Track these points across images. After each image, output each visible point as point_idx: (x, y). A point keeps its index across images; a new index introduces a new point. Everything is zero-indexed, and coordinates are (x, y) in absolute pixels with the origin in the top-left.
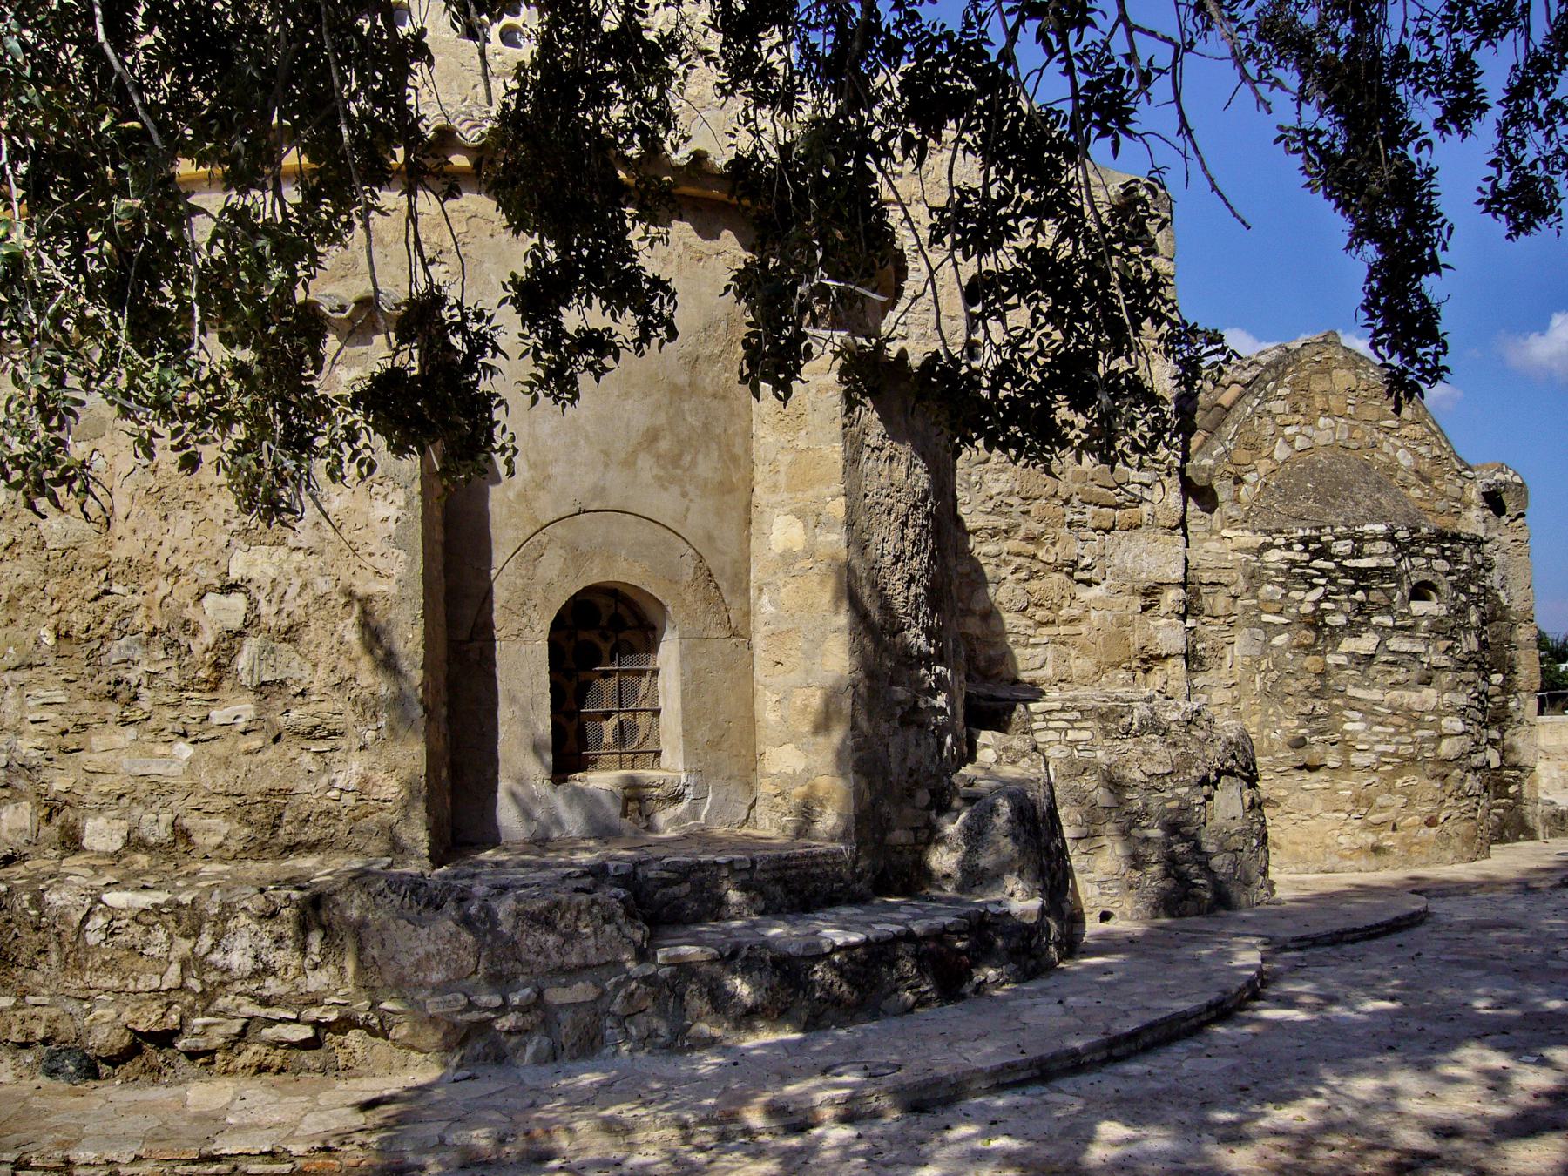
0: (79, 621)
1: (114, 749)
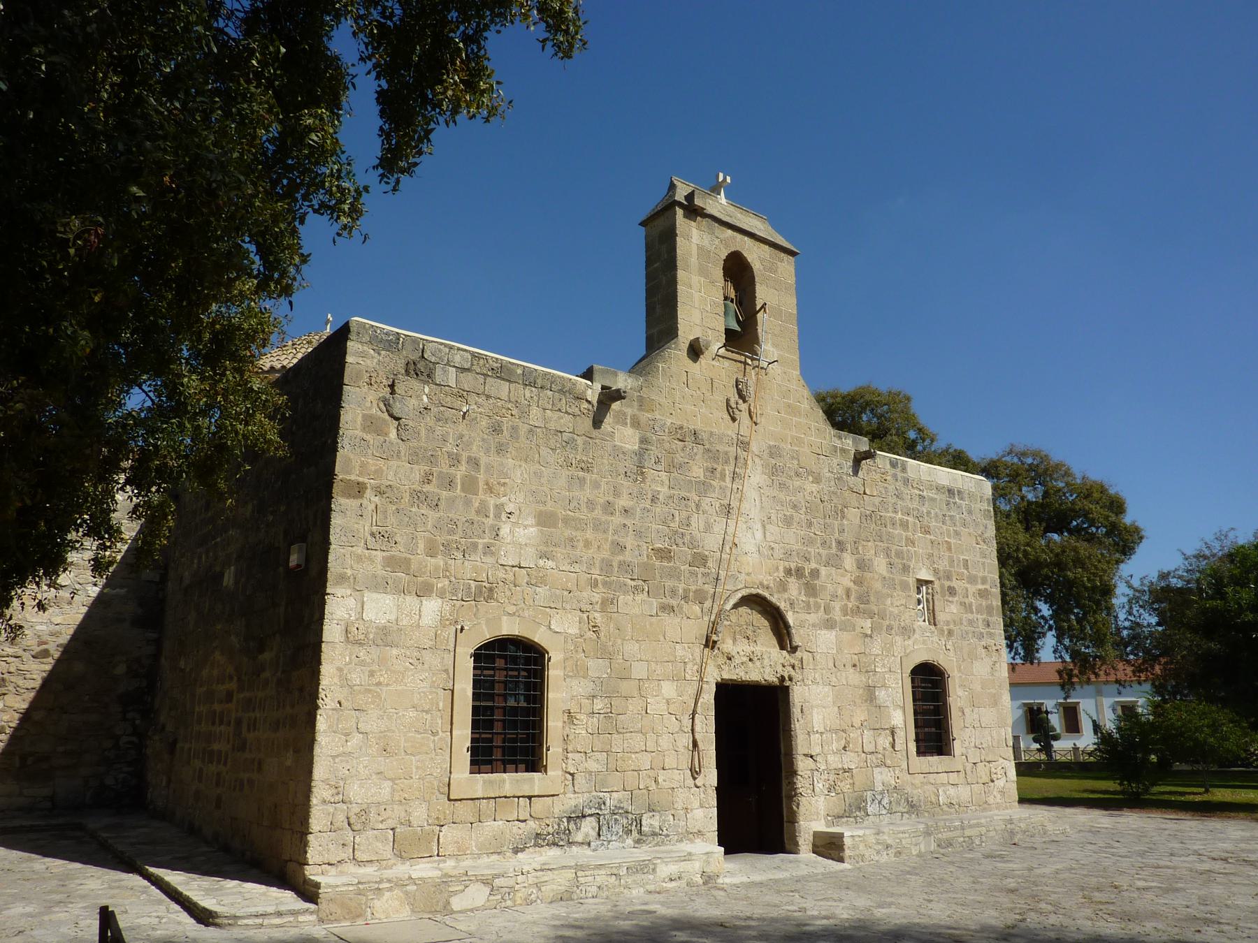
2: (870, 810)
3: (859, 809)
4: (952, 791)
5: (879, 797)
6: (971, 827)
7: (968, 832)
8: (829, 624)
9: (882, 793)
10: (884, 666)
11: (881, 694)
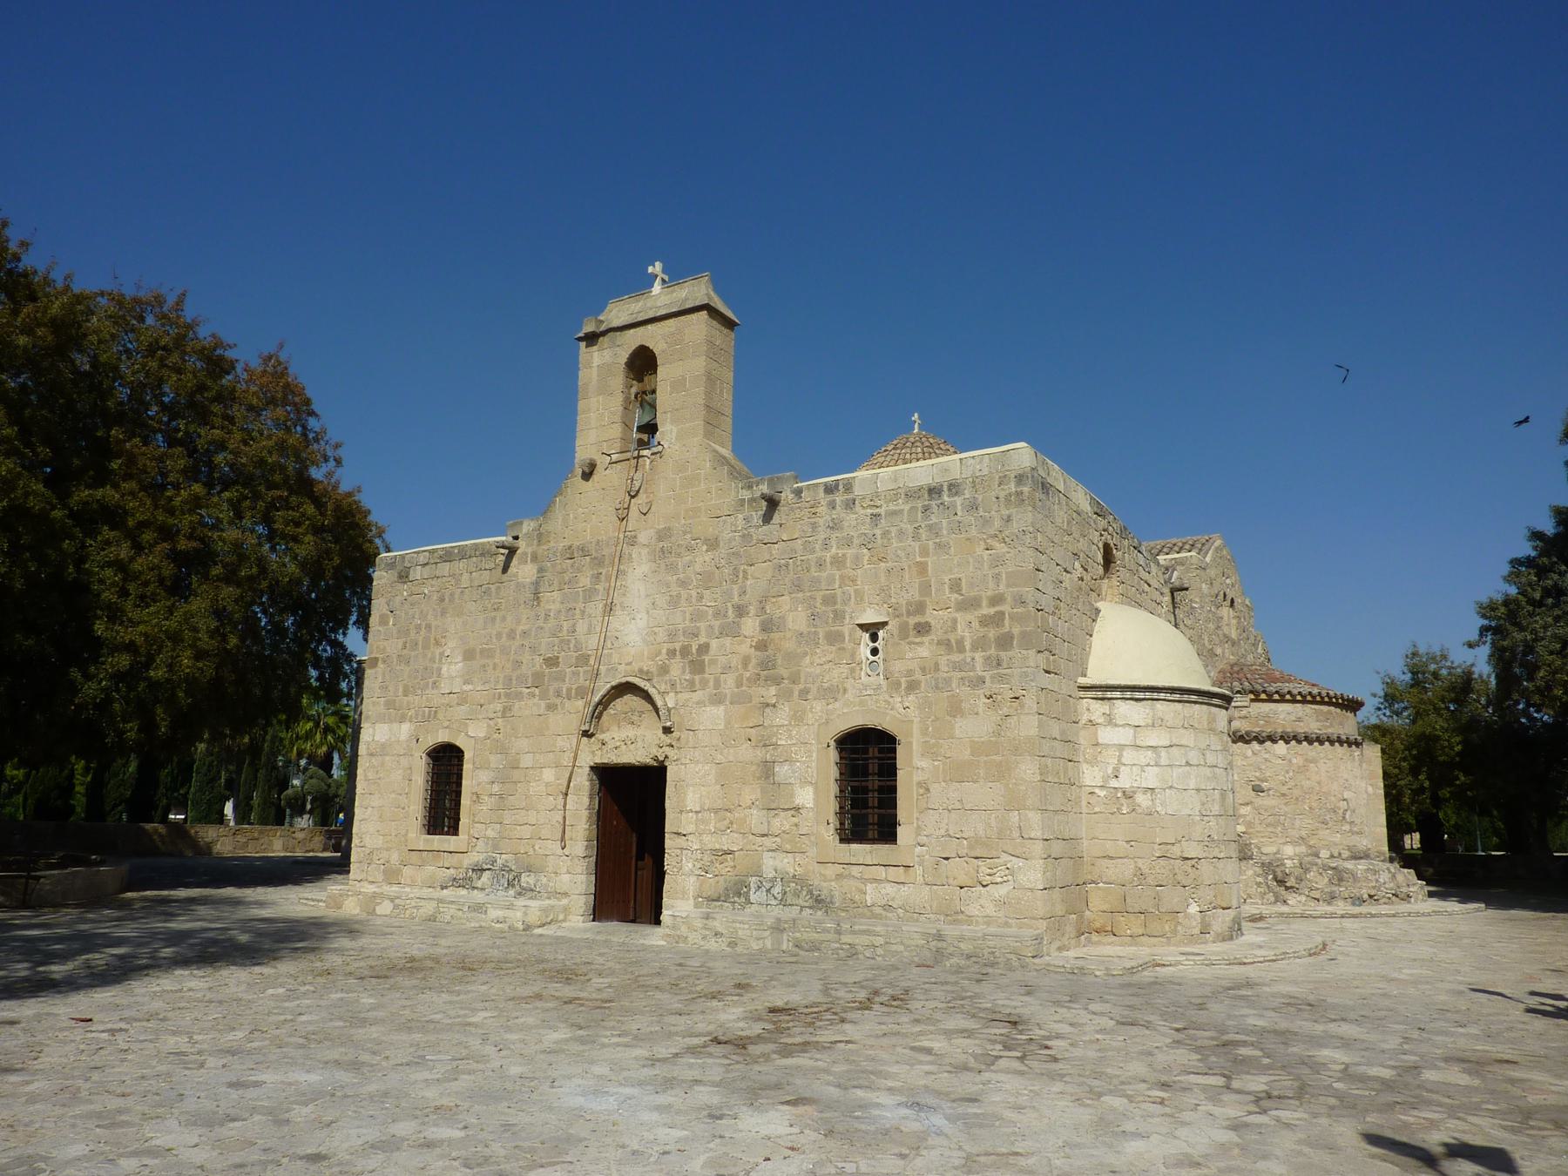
0: (1314, 805)
1: (1324, 833)
2: (753, 898)
3: (739, 895)
4: (890, 889)
5: (768, 885)
6: (854, 933)
7: (846, 939)
8: (717, 700)
9: (773, 880)
10: (790, 737)
11: (782, 771)
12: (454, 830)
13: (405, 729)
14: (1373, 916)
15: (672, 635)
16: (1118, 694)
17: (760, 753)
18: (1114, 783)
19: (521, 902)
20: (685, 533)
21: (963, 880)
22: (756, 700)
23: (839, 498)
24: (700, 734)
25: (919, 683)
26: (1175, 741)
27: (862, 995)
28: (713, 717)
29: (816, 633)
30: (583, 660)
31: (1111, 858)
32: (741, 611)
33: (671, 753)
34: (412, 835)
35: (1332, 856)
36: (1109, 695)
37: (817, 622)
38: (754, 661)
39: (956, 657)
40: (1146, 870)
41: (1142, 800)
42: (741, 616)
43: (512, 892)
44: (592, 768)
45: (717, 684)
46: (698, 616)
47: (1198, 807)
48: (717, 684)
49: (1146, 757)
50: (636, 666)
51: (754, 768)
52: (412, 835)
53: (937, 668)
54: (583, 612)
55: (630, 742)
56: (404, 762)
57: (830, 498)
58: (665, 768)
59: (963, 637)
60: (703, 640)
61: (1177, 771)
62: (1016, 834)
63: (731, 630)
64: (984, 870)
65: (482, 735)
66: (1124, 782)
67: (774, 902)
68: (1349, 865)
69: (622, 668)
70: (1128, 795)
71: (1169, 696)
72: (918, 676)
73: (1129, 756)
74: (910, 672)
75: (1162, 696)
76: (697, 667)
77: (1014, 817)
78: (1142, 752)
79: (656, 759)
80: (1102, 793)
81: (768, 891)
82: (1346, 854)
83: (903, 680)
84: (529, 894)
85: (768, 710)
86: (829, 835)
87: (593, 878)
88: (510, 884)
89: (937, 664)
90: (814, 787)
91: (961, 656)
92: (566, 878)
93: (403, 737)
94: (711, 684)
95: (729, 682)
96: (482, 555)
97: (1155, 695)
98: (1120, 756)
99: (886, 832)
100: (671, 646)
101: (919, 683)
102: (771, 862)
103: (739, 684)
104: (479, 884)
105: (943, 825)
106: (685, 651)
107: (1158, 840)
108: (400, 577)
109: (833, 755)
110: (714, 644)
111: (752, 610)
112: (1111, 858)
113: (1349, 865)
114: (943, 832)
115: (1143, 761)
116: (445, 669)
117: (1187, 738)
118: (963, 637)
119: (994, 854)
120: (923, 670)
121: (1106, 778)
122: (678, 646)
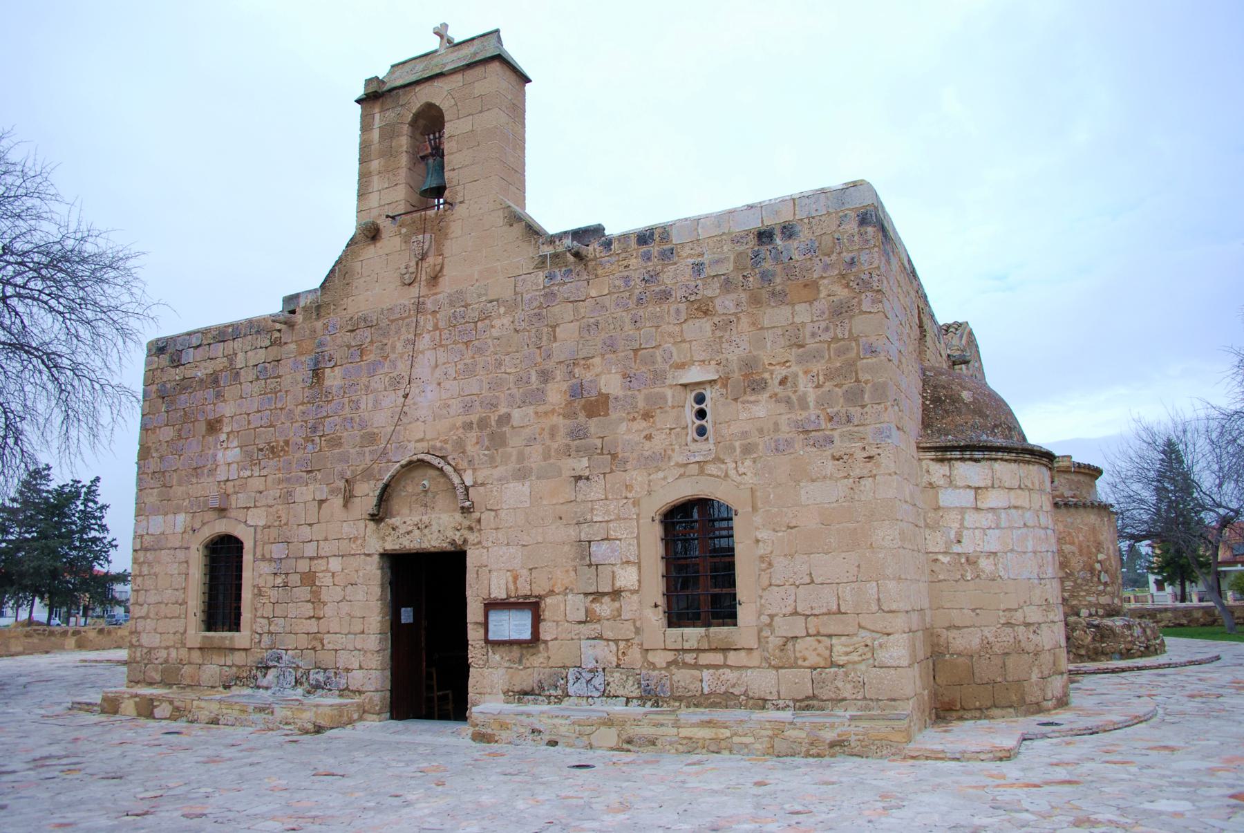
2: (571, 690)
5: (588, 676)
8: (522, 475)
12: (235, 625)
13: (181, 519)
14: (1139, 669)
15: (468, 408)
16: (957, 454)
17: (573, 533)
18: (956, 549)
19: (315, 699)
20: (479, 296)
21: (813, 659)
22: (567, 473)
23: (654, 249)
24: (502, 514)
25: (756, 445)
26: (1014, 502)
27: (29, 403)
28: (515, 494)
29: (633, 397)
30: (371, 438)
31: (958, 628)
32: (545, 376)
33: (472, 538)
34: (191, 632)
35: (1090, 615)
36: (948, 455)
37: (635, 384)
38: (562, 431)
39: (801, 415)
40: (992, 639)
41: (985, 564)
42: (546, 381)
43: (300, 690)
44: (382, 555)
45: (521, 457)
46: (495, 385)
47: (1036, 571)
48: (521, 457)
49: (986, 520)
50: (423, 446)
51: (566, 548)
52: (191, 632)
53: (776, 428)
54: (367, 387)
55: (425, 527)
56: (181, 555)
57: (644, 249)
58: (464, 553)
59: (805, 394)
60: (503, 410)
61: (1017, 533)
62: (874, 608)
63: (535, 397)
64: (838, 649)
65: (262, 523)
66: (967, 547)
67: (597, 694)
68: (1107, 622)
69: (411, 446)
70: (971, 561)
71: (1006, 456)
72: (754, 438)
73: (971, 519)
74: (745, 434)
75: (1000, 455)
76: (497, 441)
77: (872, 589)
78: (983, 514)
79: (453, 543)
80: (945, 559)
81: (588, 682)
82: (1101, 612)
83: (737, 444)
84: (320, 692)
85: (580, 483)
86: (655, 618)
87: (388, 673)
88: (298, 682)
89: (776, 424)
90: (639, 567)
91: (805, 414)
92: (358, 674)
93: (179, 529)
94: (514, 458)
95: (535, 456)
96: (258, 332)
97: (993, 455)
98: (963, 519)
99: (723, 610)
100: (467, 419)
101: (756, 445)
102: (590, 652)
103: (546, 457)
104: (264, 682)
105: (791, 601)
106: (483, 424)
107: (1002, 607)
108: (172, 361)
109: (657, 530)
110: (516, 414)
111: (559, 374)
112: (958, 628)
113: (1107, 622)
114: (789, 610)
115: (985, 524)
116: (220, 454)
117: (1021, 499)
118: (805, 394)
119: (851, 630)
120: (761, 431)
121: (948, 544)
122: (474, 418)
